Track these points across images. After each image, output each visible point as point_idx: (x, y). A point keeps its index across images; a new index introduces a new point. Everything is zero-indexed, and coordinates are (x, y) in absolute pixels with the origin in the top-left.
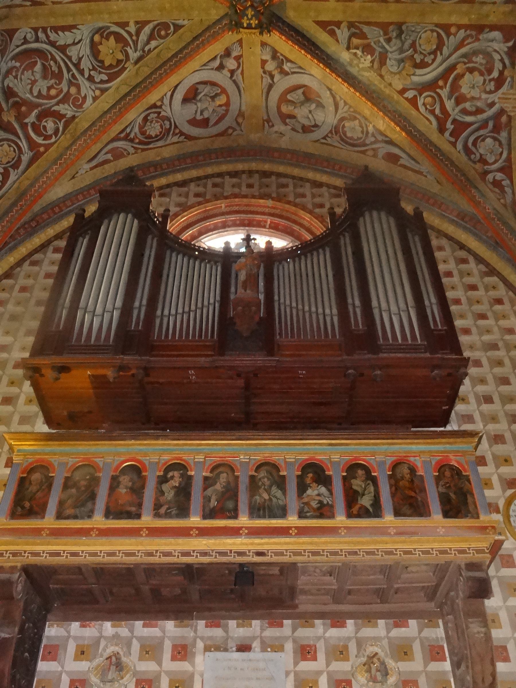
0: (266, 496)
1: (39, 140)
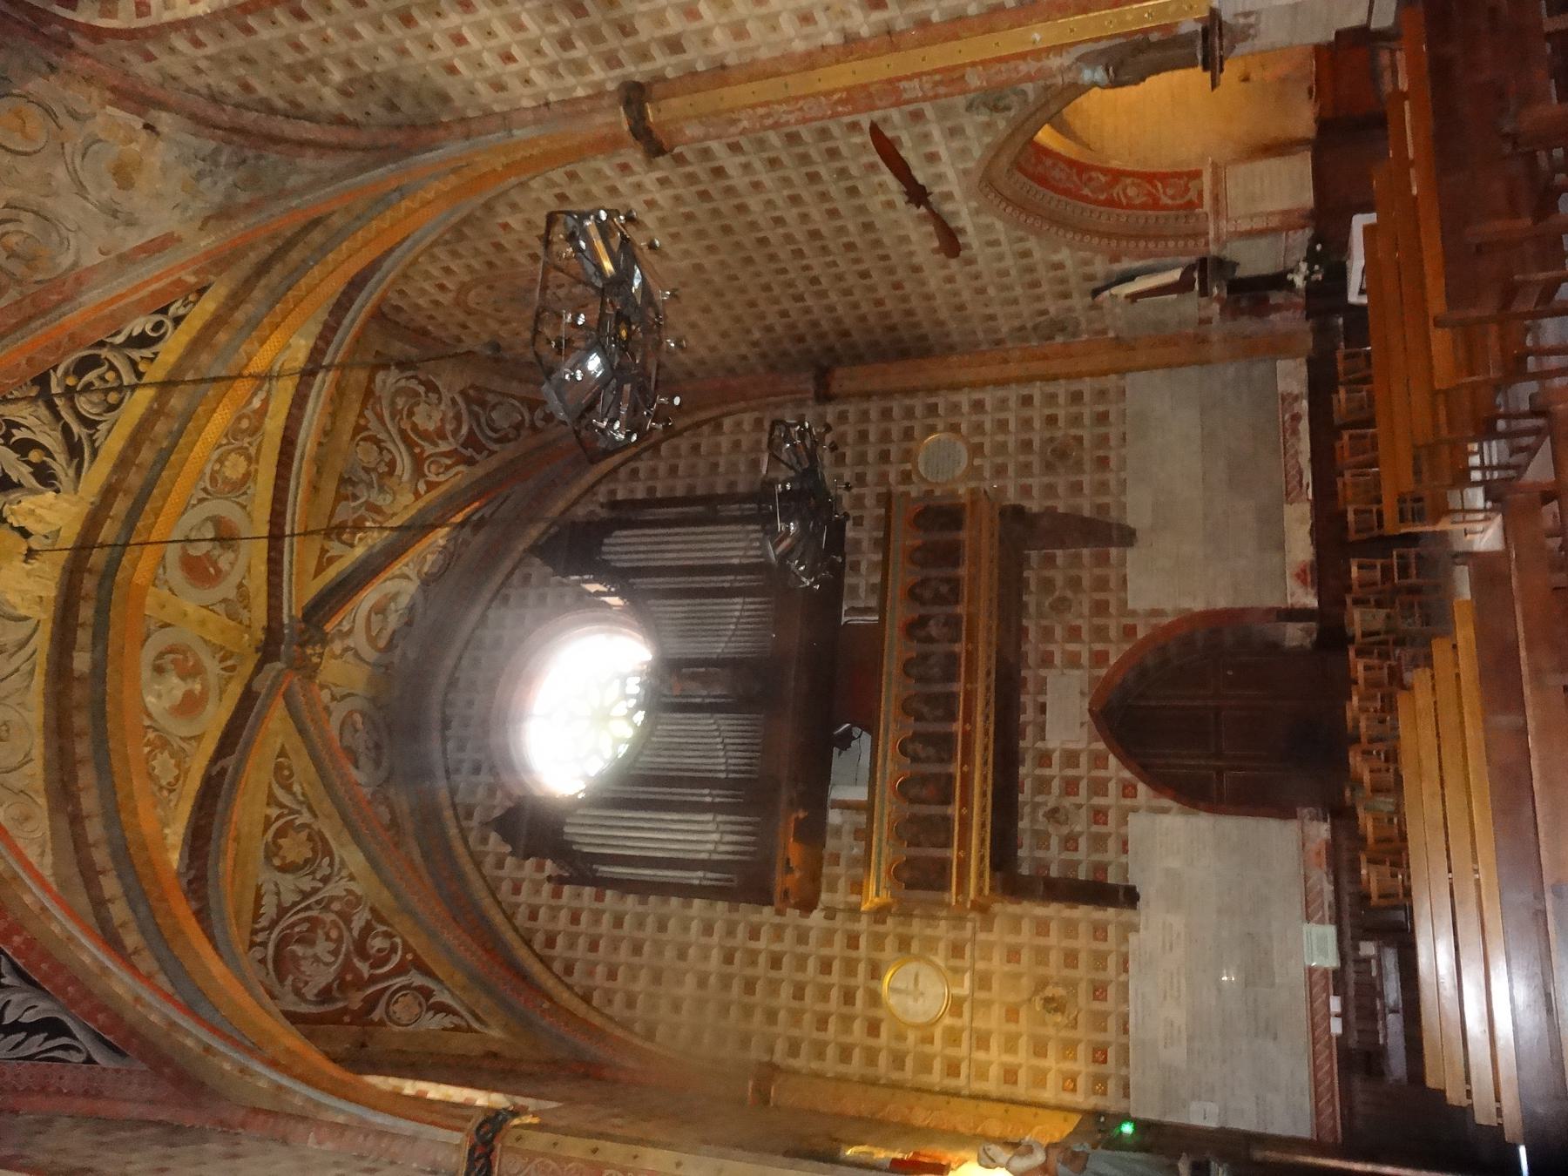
0: (936, 670)
1: (396, 959)
